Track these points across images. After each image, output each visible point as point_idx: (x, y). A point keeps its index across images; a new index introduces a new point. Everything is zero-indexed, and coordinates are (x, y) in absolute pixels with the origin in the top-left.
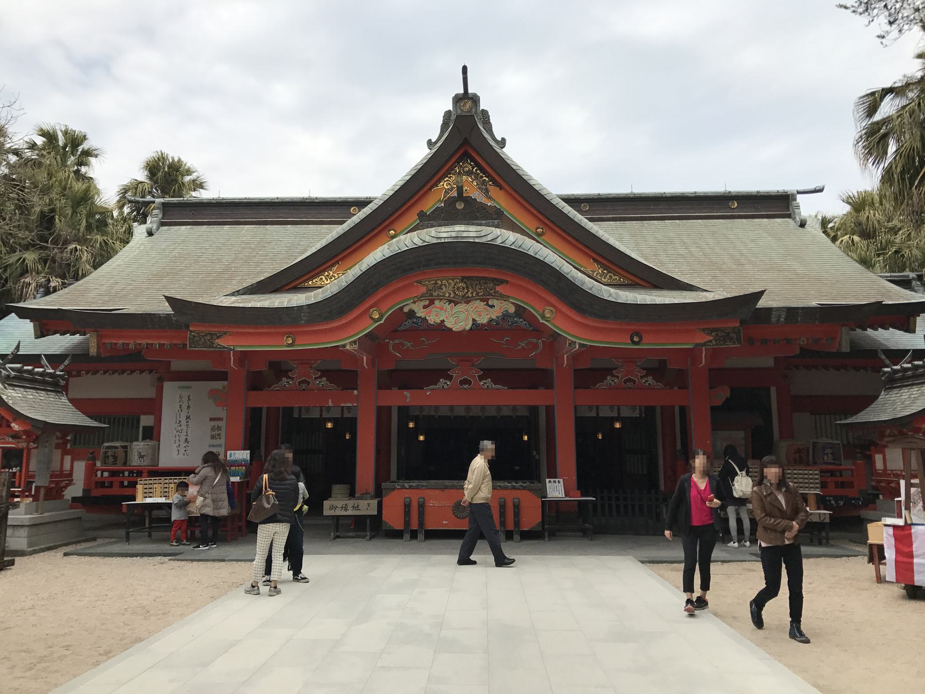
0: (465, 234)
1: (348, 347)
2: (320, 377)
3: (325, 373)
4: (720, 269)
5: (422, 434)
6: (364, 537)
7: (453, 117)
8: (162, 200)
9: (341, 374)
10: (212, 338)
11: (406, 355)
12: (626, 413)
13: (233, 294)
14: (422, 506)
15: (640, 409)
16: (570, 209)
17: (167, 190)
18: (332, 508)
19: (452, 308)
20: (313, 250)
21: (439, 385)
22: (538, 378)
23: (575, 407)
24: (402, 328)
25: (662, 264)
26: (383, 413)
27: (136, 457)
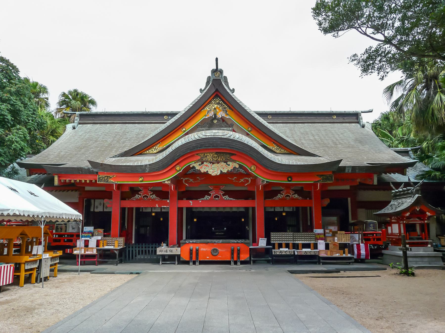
0: (217, 134)
1: (166, 182)
2: (153, 194)
3: (155, 192)
4: (327, 147)
5: (195, 218)
6: (175, 264)
7: (211, 79)
8: (79, 113)
9: (162, 193)
10: (108, 178)
11: (190, 185)
12: (286, 209)
13: (113, 157)
14: (197, 251)
15: (293, 208)
16: (263, 120)
17: (77, 104)
18: (160, 251)
19: (211, 166)
20: (149, 137)
21: (205, 198)
22: (248, 195)
23: (265, 208)
24: (189, 173)
25: (303, 144)
26: (180, 210)
27: (71, 229)
